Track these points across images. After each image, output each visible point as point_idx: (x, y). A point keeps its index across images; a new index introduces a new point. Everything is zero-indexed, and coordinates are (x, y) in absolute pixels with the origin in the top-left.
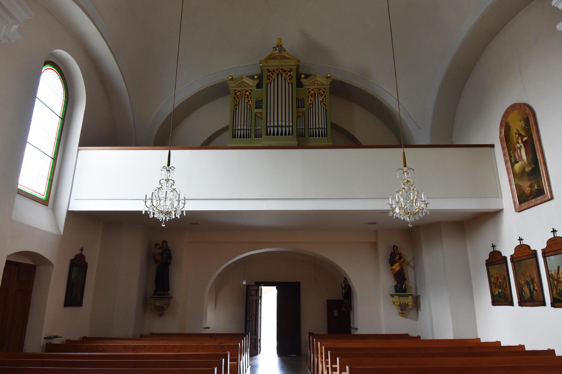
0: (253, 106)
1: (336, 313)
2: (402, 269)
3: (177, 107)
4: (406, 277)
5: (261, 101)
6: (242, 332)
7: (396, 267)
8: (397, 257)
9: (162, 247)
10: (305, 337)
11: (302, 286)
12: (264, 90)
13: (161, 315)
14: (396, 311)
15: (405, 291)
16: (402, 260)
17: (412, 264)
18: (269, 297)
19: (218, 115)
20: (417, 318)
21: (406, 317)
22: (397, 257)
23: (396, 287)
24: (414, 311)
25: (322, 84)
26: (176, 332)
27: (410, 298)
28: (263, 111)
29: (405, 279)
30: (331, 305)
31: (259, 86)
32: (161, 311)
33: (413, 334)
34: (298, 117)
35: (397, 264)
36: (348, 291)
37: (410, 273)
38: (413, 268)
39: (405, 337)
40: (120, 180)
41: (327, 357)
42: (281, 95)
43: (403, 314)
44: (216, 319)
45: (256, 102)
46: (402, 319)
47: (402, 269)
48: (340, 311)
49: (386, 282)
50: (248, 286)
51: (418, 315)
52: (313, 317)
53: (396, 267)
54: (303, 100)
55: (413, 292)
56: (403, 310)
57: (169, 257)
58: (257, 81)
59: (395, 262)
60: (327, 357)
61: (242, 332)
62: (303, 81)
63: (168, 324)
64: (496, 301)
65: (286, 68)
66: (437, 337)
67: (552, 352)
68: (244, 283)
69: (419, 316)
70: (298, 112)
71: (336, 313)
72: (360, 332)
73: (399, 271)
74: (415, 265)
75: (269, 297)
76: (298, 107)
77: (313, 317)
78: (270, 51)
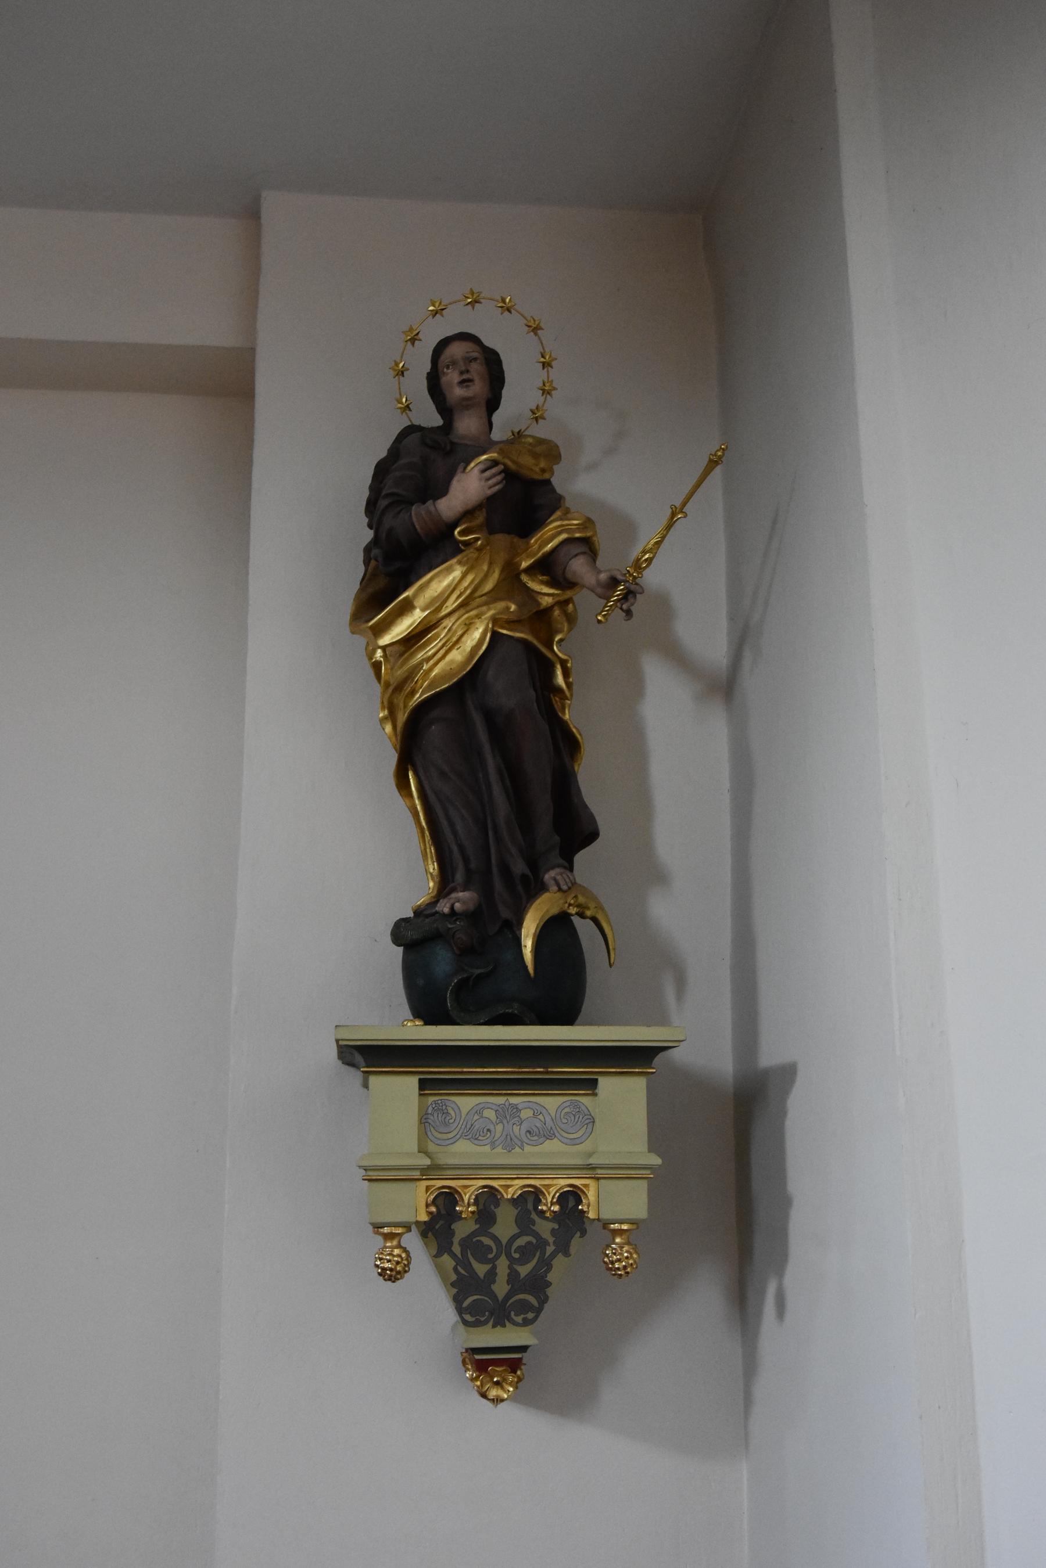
3: (571, 921)
4: (595, 782)
8: (470, 486)
15: (558, 990)
16: (549, 537)
17: (688, 579)
20: (734, 1408)
21: (572, 1401)
22: (470, 486)
23: (415, 936)
24: (701, 1302)
29: (576, 831)
35: (444, 582)
37: (659, 753)
38: (724, 688)
43: (491, 1367)
46: (508, 1428)
51: (750, 1367)
53: (452, 618)
55: (699, 1037)
69: (761, 1389)
73: (471, 681)
74: (744, 636)
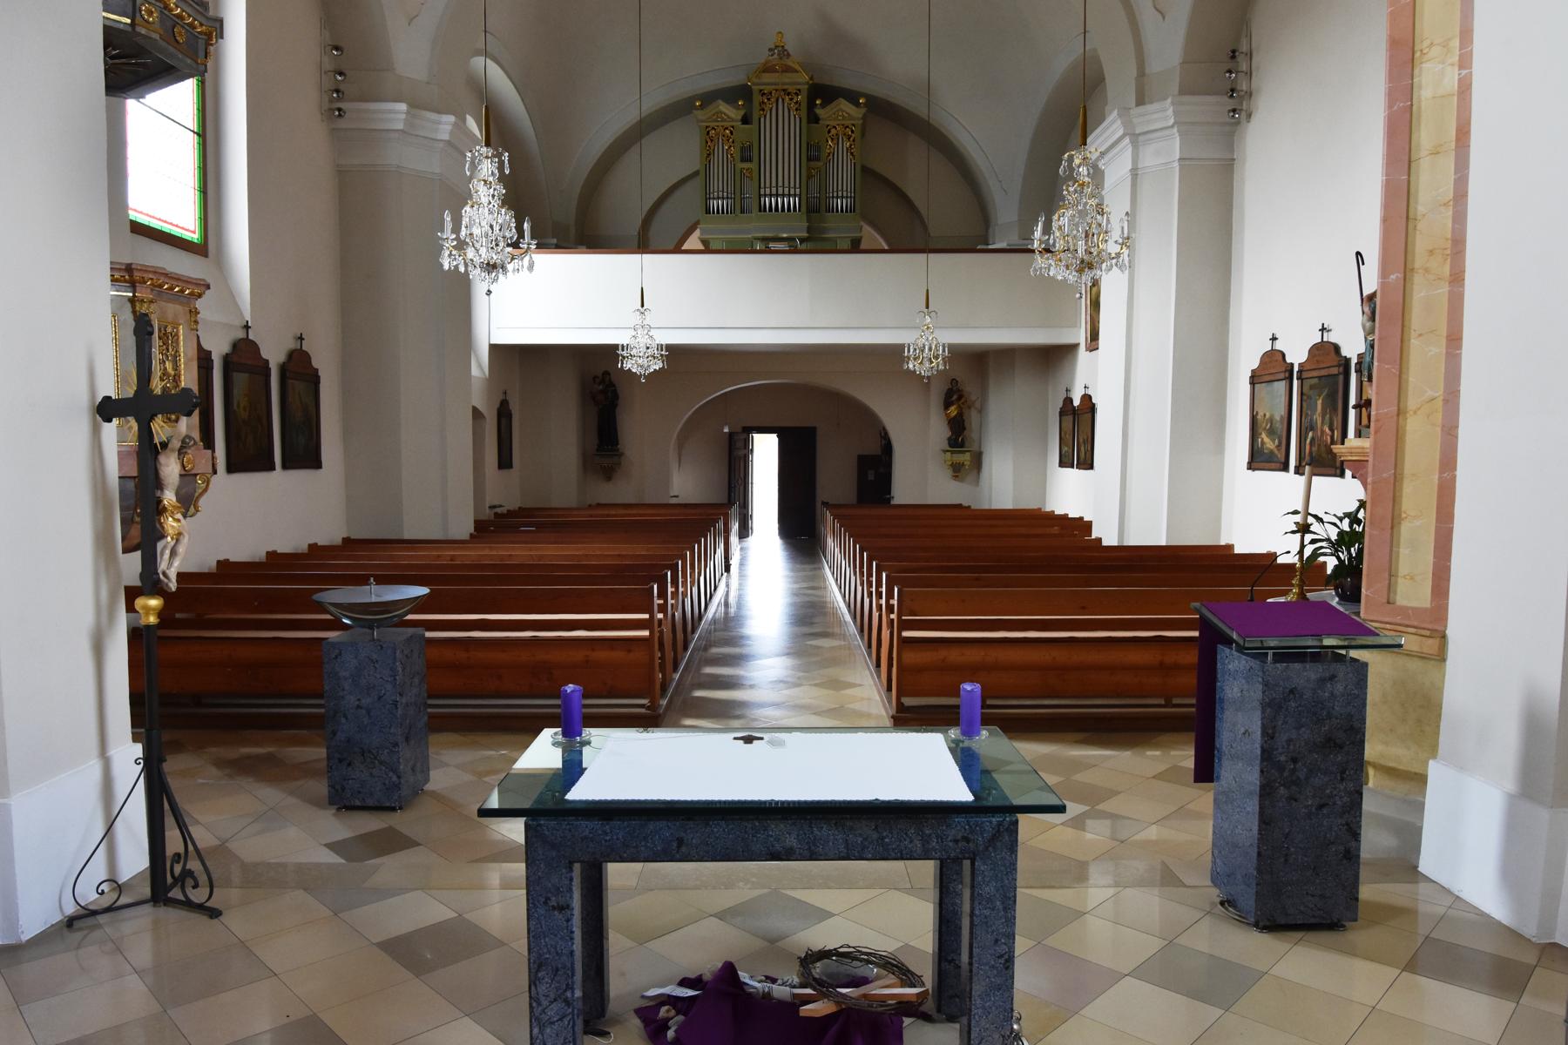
0: (738, 157)
1: (871, 476)
2: (960, 414)
5: (750, 147)
6: (717, 497)
7: (953, 411)
9: (603, 381)
10: (819, 505)
11: (819, 433)
12: (754, 127)
13: (609, 478)
14: (950, 472)
17: (978, 404)
18: (765, 451)
19: (674, 155)
20: (977, 481)
25: (851, 117)
26: (633, 501)
27: (967, 456)
28: (753, 166)
30: (864, 463)
31: (746, 120)
32: (608, 473)
33: (965, 504)
34: (809, 177)
36: (888, 448)
37: (973, 418)
39: (959, 506)
40: (548, 300)
41: (879, 584)
42: (781, 135)
44: (686, 484)
45: (742, 149)
47: (960, 414)
48: (876, 469)
49: (938, 431)
50: (731, 434)
52: (835, 477)
53: (953, 411)
54: (818, 148)
56: (957, 471)
57: (616, 396)
58: (742, 112)
59: (951, 404)
60: (879, 584)
61: (717, 497)
62: (819, 111)
63: (620, 492)
64: (1062, 464)
65: (791, 89)
66: (986, 507)
67: (1081, 518)
68: (726, 430)
70: (809, 169)
71: (871, 476)
72: (894, 502)
75: (765, 451)
76: (809, 159)
77: (835, 477)
78: (762, 57)
